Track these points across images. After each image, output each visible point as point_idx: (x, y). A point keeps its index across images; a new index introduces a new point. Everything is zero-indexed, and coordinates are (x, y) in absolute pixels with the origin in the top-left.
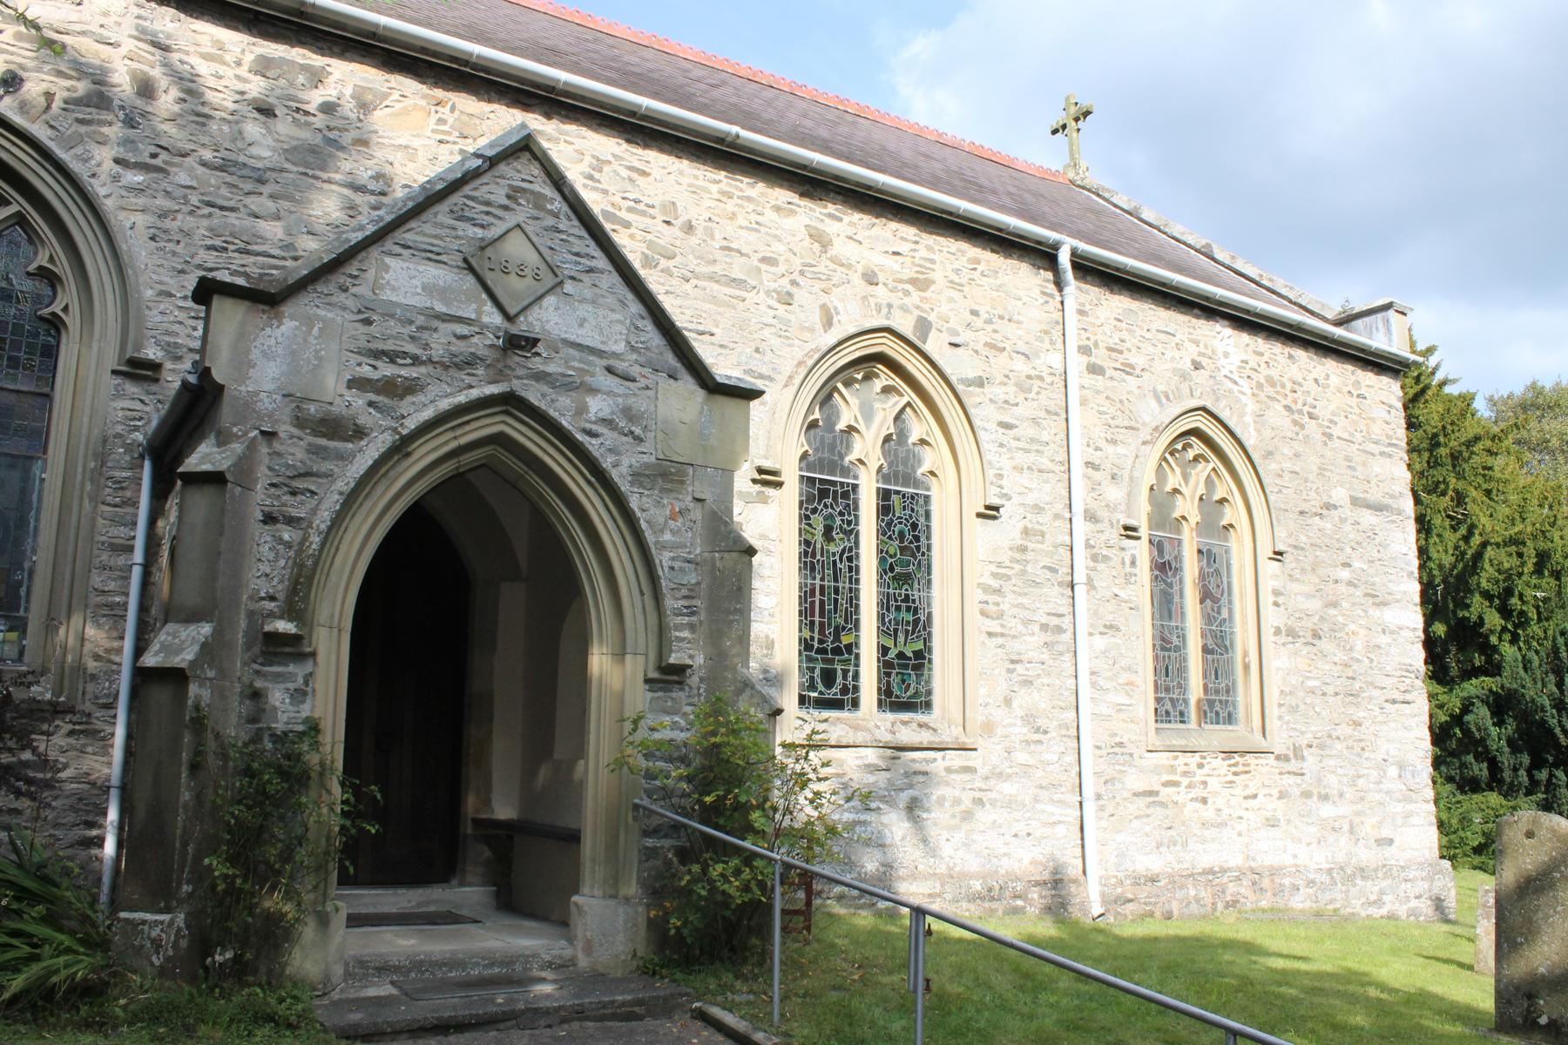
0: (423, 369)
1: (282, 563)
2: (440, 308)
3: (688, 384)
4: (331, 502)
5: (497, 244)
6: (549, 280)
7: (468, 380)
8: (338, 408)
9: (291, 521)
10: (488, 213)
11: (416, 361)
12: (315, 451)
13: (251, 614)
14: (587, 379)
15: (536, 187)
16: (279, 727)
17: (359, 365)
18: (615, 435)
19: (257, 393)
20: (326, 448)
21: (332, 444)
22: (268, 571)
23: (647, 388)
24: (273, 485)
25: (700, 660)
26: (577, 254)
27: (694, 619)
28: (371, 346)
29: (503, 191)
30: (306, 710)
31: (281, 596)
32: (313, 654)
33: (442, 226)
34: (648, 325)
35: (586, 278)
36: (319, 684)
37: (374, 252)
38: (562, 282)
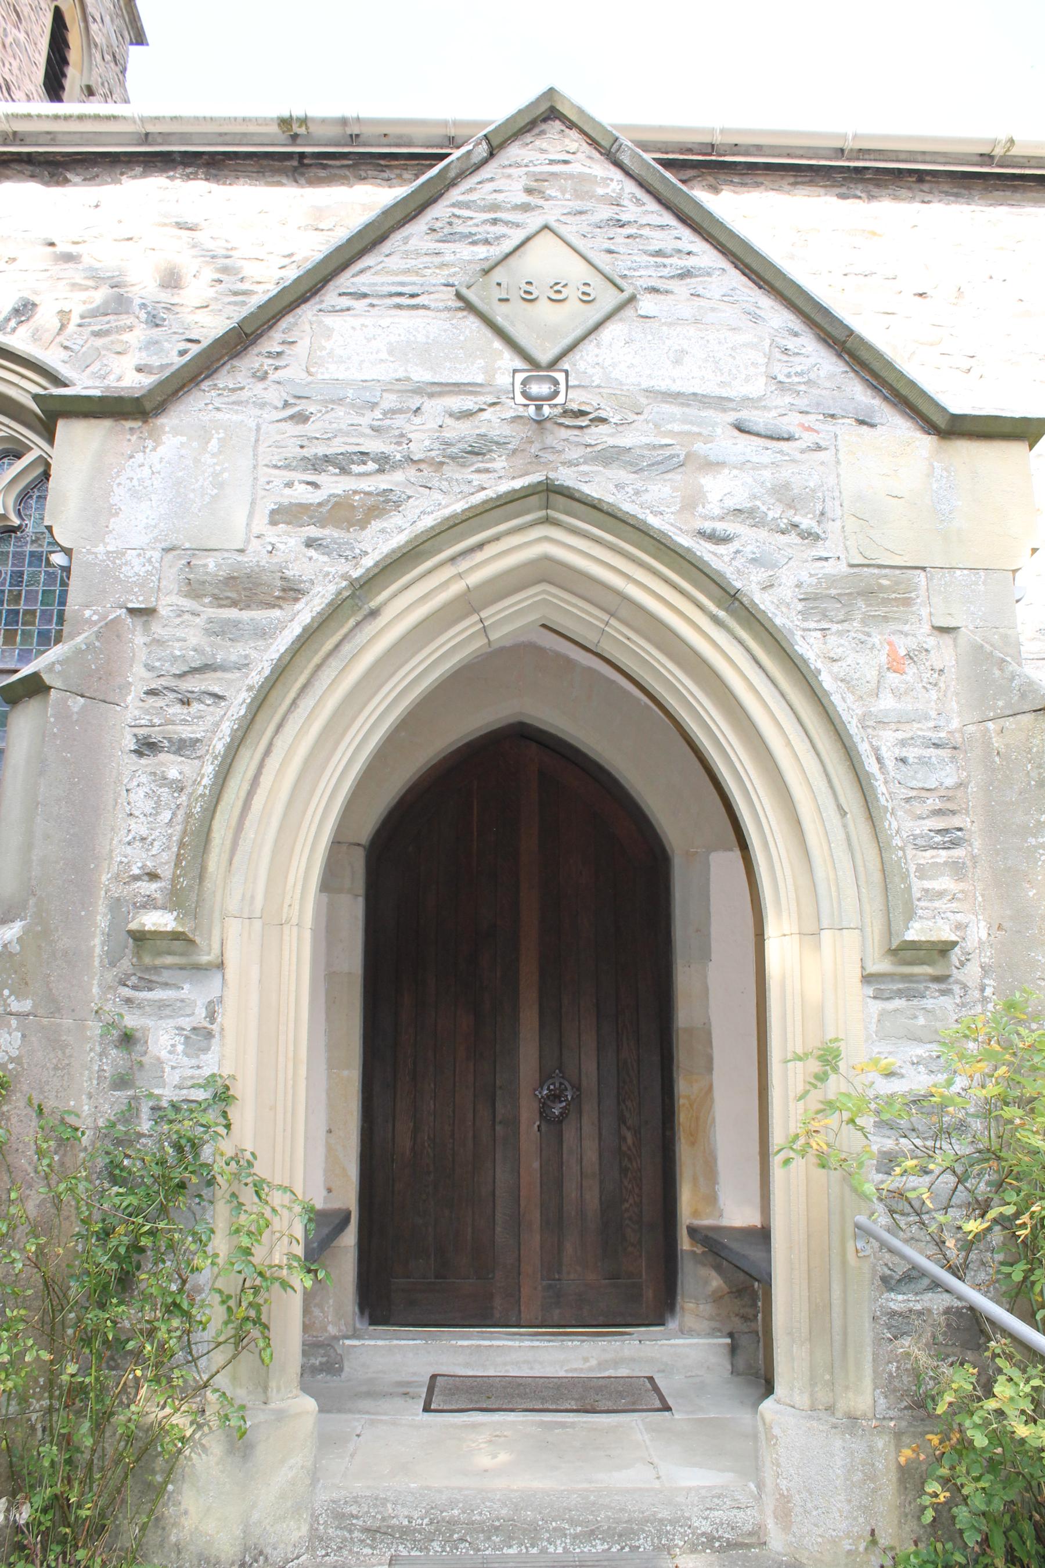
0: (398, 476)
1: (166, 816)
2: (421, 375)
3: (898, 428)
4: (239, 702)
5: (512, 260)
6: (609, 298)
7: (478, 479)
8: (256, 556)
9: (182, 747)
10: (495, 222)
11: (384, 464)
12: (221, 630)
13: (116, 905)
14: (700, 447)
15: (575, 168)
16: (167, 1094)
17: (289, 485)
18: (763, 534)
19: (122, 553)
20: (236, 624)
21: (246, 615)
22: (144, 831)
23: (819, 448)
24: (152, 693)
25: (978, 932)
26: (659, 253)
27: (958, 853)
28: (306, 453)
29: (518, 186)
30: (210, 1064)
31: (166, 872)
33: (417, 254)
34: (808, 345)
35: (681, 288)
36: (227, 1018)
37: (307, 312)
38: (632, 299)
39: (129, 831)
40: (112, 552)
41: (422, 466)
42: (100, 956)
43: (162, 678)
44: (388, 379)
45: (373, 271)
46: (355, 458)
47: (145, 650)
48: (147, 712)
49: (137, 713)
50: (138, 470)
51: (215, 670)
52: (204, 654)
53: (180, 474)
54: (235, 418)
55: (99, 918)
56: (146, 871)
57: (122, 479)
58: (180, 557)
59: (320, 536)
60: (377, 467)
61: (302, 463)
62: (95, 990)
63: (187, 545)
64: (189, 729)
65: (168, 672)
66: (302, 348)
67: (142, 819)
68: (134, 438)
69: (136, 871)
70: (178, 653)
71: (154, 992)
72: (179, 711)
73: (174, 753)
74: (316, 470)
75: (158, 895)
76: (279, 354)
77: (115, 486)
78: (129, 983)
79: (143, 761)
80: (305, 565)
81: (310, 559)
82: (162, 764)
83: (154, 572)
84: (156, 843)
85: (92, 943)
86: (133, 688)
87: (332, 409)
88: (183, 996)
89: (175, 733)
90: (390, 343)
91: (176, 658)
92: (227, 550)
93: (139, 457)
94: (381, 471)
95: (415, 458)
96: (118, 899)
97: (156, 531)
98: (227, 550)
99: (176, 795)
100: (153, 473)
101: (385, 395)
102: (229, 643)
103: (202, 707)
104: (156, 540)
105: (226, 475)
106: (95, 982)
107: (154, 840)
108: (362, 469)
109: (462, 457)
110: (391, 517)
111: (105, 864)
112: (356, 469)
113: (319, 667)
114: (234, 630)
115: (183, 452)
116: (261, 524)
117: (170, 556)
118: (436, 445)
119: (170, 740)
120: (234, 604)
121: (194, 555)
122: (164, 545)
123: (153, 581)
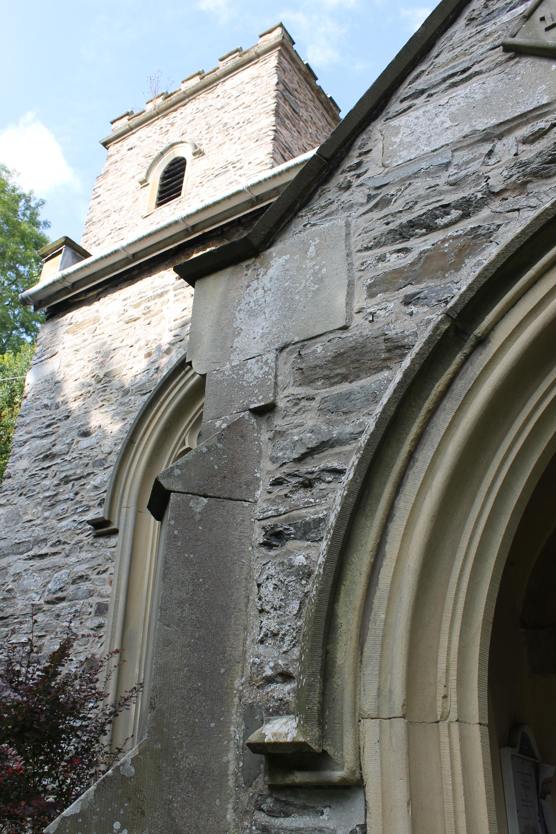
0: (485, 212)
1: (295, 606)
2: (483, 123)
8: (361, 327)
11: (467, 208)
17: (382, 259)
20: (348, 396)
21: (356, 385)
22: (273, 626)
24: (277, 482)
28: (391, 226)
32: (352, 787)
37: (378, 126)
39: (261, 628)
40: (236, 366)
41: (506, 195)
42: (235, 774)
43: (285, 466)
44: (455, 139)
45: (426, 73)
46: (438, 212)
47: (270, 445)
48: (273, 502)
49: (264, 505)
50: (254, 294)
51: (332, 446)
52: (320, 433)
53: (287, 284)
54: (327, 225)
55: (232, 728)
56: (279, 671)
57: (242, 306)
58: (291, 353)
59: (417, 291)
60: (460, 212)
61: (390, 236)
62: (230, 816)
63: (296, 339)
64: (312, 510)
65: (289, 458)
66: (376, 154)
67: (273, 613)
68: (250, 272)
69: (269, 672)
70: (296, 438)
71: (290, 819)
72: (302, 495)
73: (301, 539)
74: (404, 237)
75: (290, 698)
76: (359, 165)
77: (237, 313)
78: (264, 807)
79: (272, 553)
80: (406, 323)
81: (411, 314)
82: (290, 552)
83: (270, 371)
84: (287, 638)
85: (225, 759)
86: (261, 483)
87: (410, 184)
88: (321, 824)
89: (300, 518)
90: (452, 113)
91: (295, 443)
92: (331, 332)
93: (255, 284)
94: (466, 215)
95: (496, 190)
96: (251, 706)
97: (270, 336)
98: (331, 332)
99: (304, 582)
100: (265, 292)
101: (456, 154)
102: (344, 417)
103: (323, 486)
104: (270, 343)
105: (324, 270)
106: (230, 806)
107: (284, 635)
108: (447, 219)
109: (544, 169)
110: (484, 249)
111: (239, 668)
112: (440, 222)
113: (432, 413)
114: (347, 403)
115: (288, 266)
116: (360, 299)
117: (284, 354)
118: (514, 171)
119: (295, 525)
120: (345, 378)
121: (303, 346)
122: (277, 346)
123: (270, 379)
